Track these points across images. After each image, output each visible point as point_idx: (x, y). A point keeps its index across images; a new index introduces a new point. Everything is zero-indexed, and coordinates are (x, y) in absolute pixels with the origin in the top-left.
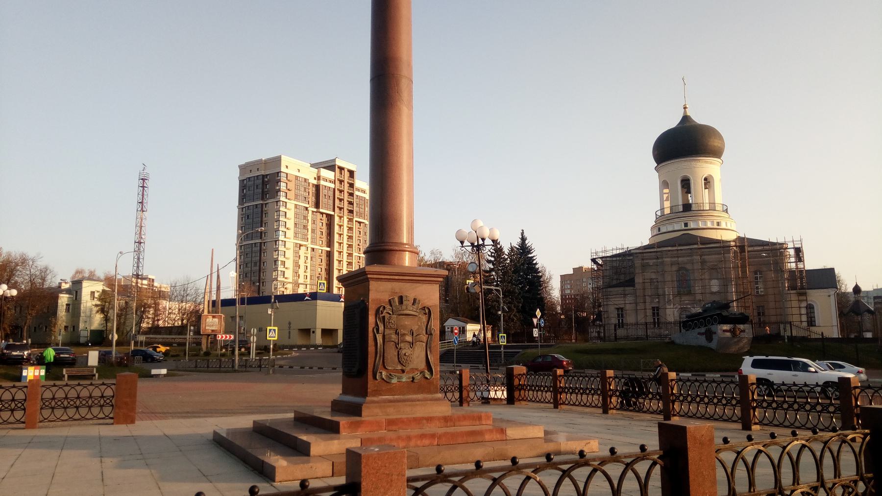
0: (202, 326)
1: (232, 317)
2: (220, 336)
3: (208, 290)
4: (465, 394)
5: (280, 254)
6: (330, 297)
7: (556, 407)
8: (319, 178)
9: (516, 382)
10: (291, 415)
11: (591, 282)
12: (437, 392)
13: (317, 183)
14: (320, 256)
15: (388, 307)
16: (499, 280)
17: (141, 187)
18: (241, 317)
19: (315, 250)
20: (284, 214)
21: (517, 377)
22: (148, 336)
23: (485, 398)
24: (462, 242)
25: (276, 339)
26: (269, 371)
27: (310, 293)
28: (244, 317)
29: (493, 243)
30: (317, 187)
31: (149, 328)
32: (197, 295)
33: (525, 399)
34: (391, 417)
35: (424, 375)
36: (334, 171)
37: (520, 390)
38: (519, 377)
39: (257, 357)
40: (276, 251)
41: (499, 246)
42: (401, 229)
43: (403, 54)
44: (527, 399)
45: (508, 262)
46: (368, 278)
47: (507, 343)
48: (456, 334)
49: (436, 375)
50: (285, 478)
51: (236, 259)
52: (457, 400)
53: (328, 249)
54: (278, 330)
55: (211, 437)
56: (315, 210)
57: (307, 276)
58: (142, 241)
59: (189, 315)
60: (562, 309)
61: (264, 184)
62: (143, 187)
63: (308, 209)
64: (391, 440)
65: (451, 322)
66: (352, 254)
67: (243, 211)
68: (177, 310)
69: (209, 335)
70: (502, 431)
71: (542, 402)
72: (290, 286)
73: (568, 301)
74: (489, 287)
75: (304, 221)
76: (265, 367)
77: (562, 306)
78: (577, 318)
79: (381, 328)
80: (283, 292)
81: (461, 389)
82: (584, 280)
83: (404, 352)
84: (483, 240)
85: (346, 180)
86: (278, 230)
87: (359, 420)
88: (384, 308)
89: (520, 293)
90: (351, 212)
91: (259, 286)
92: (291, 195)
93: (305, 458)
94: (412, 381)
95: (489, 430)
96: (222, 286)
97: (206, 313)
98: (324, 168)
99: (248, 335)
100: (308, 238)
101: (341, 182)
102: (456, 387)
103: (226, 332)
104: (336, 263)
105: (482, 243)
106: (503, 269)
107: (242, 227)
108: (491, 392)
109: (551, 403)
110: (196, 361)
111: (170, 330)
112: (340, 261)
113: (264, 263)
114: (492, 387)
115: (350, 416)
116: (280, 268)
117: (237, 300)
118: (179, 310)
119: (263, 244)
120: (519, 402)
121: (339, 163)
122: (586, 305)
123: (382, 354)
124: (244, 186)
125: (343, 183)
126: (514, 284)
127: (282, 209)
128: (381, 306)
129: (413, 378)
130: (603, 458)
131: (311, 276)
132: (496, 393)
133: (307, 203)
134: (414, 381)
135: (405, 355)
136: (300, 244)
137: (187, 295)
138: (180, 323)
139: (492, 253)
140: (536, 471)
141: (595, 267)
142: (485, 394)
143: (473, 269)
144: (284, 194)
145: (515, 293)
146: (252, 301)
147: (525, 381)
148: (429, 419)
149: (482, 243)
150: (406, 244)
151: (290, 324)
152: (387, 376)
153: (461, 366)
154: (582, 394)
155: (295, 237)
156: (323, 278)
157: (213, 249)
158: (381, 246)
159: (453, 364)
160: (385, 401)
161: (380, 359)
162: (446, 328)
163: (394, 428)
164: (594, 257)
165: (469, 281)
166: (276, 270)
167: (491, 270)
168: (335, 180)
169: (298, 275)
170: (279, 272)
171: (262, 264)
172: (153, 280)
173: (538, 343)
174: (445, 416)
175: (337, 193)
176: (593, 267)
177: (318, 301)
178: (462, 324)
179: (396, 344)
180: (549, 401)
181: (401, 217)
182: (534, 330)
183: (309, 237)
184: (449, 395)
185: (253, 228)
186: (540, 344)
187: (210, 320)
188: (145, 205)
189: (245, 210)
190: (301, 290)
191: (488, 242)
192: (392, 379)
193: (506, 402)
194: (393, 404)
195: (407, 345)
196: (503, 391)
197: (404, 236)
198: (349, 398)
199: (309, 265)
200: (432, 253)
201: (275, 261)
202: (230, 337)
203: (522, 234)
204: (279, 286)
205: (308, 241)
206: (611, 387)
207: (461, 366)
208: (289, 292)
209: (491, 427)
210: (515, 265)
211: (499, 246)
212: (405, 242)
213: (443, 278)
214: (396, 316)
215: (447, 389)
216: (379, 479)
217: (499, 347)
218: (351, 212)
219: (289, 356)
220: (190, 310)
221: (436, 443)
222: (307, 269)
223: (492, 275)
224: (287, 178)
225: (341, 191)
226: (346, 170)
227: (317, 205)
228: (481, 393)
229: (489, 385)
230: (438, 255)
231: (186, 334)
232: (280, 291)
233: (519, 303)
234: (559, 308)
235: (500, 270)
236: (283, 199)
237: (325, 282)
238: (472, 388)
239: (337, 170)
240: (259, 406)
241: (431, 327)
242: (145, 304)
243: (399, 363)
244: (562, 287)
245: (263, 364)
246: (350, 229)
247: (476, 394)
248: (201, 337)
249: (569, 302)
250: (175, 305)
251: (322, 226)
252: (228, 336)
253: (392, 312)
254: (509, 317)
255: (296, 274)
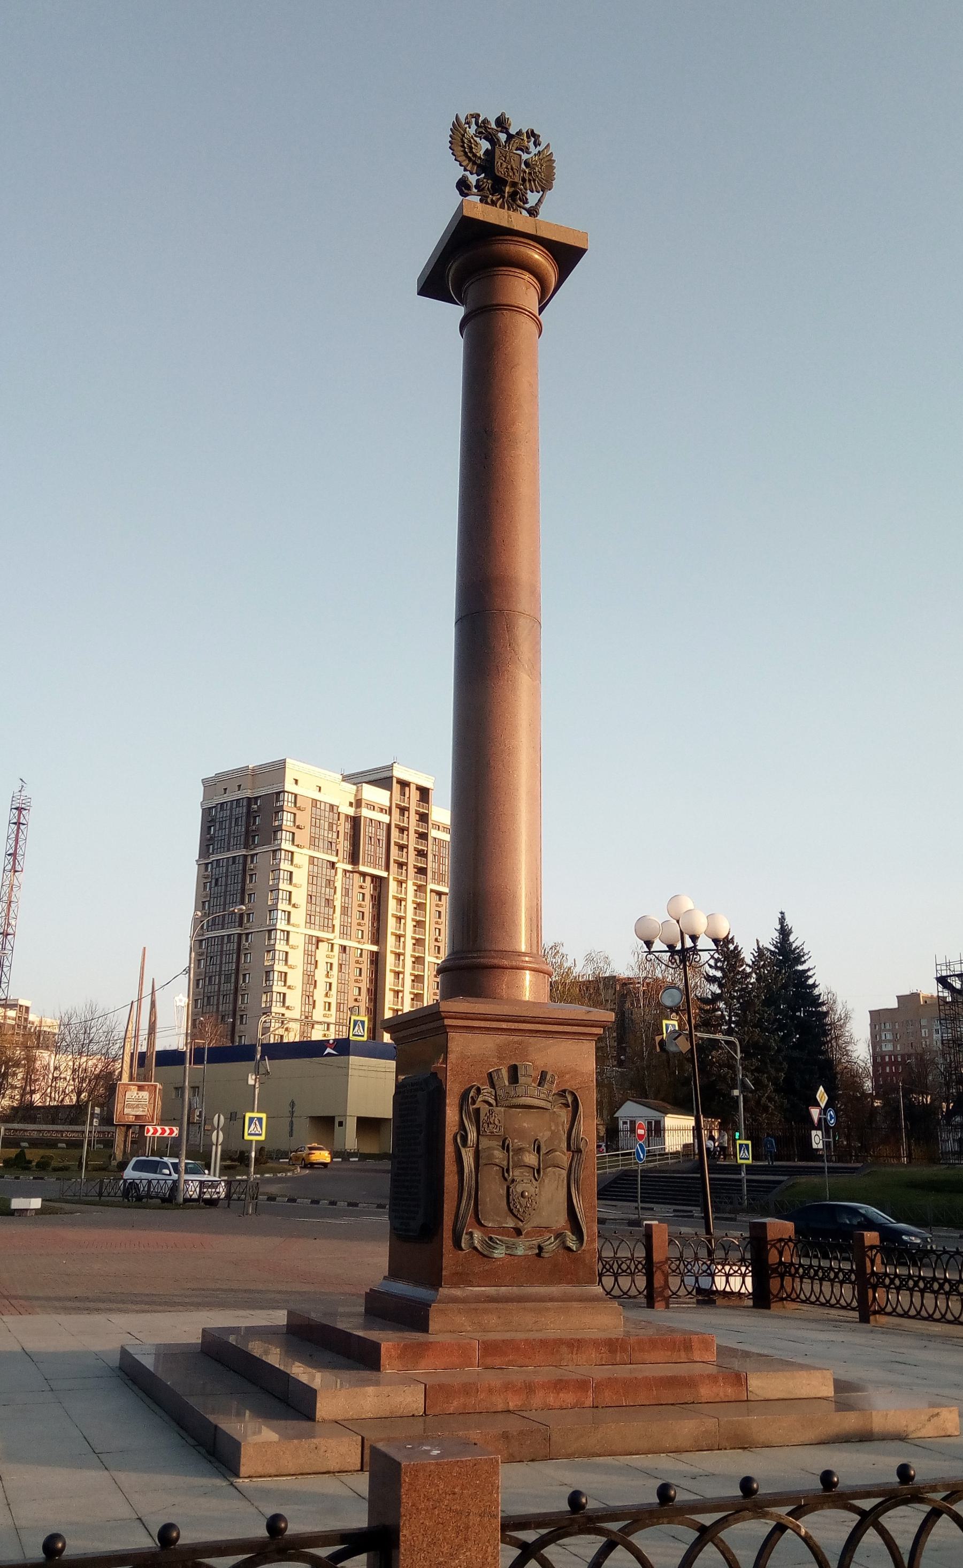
0: (118, 1107)
1: (176, 1088)
2: (150, 1128)
3: (131, 1033)
4: (658, 1280)
5: (277, 957)
6: (372, 1050)
7: (864, 1319)
8: (358, 803)
9: (773, 1257)
10: (280, 1318)
11: (939, 1027)
12: (592, 1282)
13: (356, 812)
14: (357, 962)
15: (486, 1089)
16: (733, 1019)
17: (15, 823)
18: (194, 1089)
19: (348, 949)
20: (287, 875)
21: (774, 1246)
22: (10, 1126)
23: (705, 1290)
24: (649, 944)
25: (262, 1138)
26: (245, 1207)
27: (335, 1040)
28: (201, 1089)
29: (716, 945)
30: (355, 821)
31: (13, 1108)
32: (110, 1042)
33: (794, 1296)
34: (492, 1336)
35: (564, 1242)
36: (389, 788)
37: (782, 1276)
38: (778, 1245)
39: (224, 1175)
40: (269, 951)
41: (731, 947)
42: (515, 923)
43: (522, 573)
44: (798, 1297)
45: (753, 980)
46: (445, 1026)
47: (753, 1159)
48: (641, 1137)
49: (591, 1243)
50: (260, 1470)
51: (189, 970)
52: (640, 1293)
53: (375, 948)
54: (267, 1118)
55: (115, 1361)
56: (349, 867)
57: (329, 1004)
58: (10, 931)
59: (93, 1083)
60: (876, 1087)
61: (250, 815)
62: (18, 824)
63: (337, 865)
64: (491, 1391)
65: (630, 1110)
66: (424, 958)
67: (206, 870)
68: (69, 1072)
69: (129, 1127)
70: (739, 1380)
71: (832, 1306)
72: (295, 1026)
73: (888, 1070)
74: (711, 1036)
75: (328, 890)
76: (239, 1199)
77: (876, 1077)
78: (910, 1106)
79: (472, 1136)
80: (282, 1036)
81: (649, 1268)
82: (924, 1023)
83: (519, 1189)
84: (694, 938)
85: (413, 807)
86: (273, 909)
87: (421, 1339)
88: (479, 1091)
89: (779, 1050)
90: (422, 871)
91: (234, 1024)
92: (303, 837)
93: (306, 1425)
94: (539, 1255)
95: (709, 1376)
96: (159, 1024)
97: (125, 1079)
98: (369, 783)
99: (207, 1127)
100: (334, 926)
101: (403, 810)
102: (640, 1262)
103: (163, 1121)
104: (389, 978)
105: (692, 945)
106: (740, 997)
107: (204, 902)
108: (717, 1279)
109: (853, 1309)
110: (102, 1182)
111: (54, 1114)
112: (397, 974)
113: (244, 975)
114: (720, 1267)
115: (401, 1330)
116: (278, 987)
117: (188, 1054)
118: (74, 1071)
119: (244, 937)
120: (779, 1304)
121: (399, 772)
122: (930, 1078)
123: (473, 1193)
124: (210, 819)
125: (406, 813)
126: (767, 1030)
127: (284, 865)
128: (472, 1087)
129: (540, 1248)
130: (955, 1485)
131: (339, 1004)
132: (727, 1281)
133: (335, 853)
134: (542, 1254)
135: (522, 1195)
136: (318, 937)
137: (90, 1042)
138: (75, 1099)
139: (717, 960)
140: (797, 1513)
141: (946, 994)
142: (704, 1282)
143: (672, 1001)
144: (289, 836)
145: (769, 1049)
146: (219, 1055)
147: (792, 1256)
148: (576, 1345)
149: (692, 945)
150: (525, 954)
151: (293, 1104)
152: (483, 1241)
153: (652, 1209)
154: (922, 1292)
155: (309, 923)
156: (363, 1010)
157: (145, 948)
158: (474, 958)
159: (635, 1204)
160: (478, 1299)
161: (468, 1204)
162: (621, 1123)
163: (497, 1361)
164: (944, 974)
165: (668, 1022)
166: (269, 990)
167: (716, 998)
168: (390, 808)
169: (311, 1002)
170: (275, 994)
171: (241, 977)
172: (27, 1008)
173: (823, 1161)
174: (610, 1339)
175: (395, 833)
176: (941, 994)
177: (351, 1058)
178: (653, 1114)
179: (505, 1171)
180: (849, 1305)
181: (515, 897)
182: (814, 1133)
183: (337, 923)
184: (625, 1282)
185: (225, 904)
186: (826, 1164)
187: (133, 1094)
188: (19, 858)
189: (212, 869)
190: (317, 1035)
191: (705, 943)
192: (495, 1248)
193: (750, 1303)
194: (495, 1305)
195: (528, 1175)
196: (744, 1276)
197: (520, 937)
198: (402, 1288)
199: (334, 981)
200: (589, 959)
201: (266, 972)
202: (172, 1132)
203: (782, 920)
204: (273, 1025)
205: (333, 931)
206: (875, 1269)
207: (652, 1209)
208: (292, 1036)
209: (712, 1370)
210: (768, 987)
211: (731, 947)
212: (523, 950)
213: (604, 1027)
214: (503, 1109)
215: (619, 1267)
216: (439, 1523)
217: (737, 1168)
218: (422, 871)
219: (289, 1174)
220: (96, 1073)
221: (589, 1402)
222: (330, 989)
223: (719, 1009)
224: (295, 803)
225: (402, 830)
226: (413, 787)
227: (354, 858)
228: (693, 1278)
229: (712, 1261)
230: (601, 965)
231: (84, 1123)
232: (275, 1035)
233: (778, 1070)
234: (868, 1085)
235: (734, 997)
236: (286, 845)
237: (366, 1019)
238: (673, 1266)
239: (396, 787)
240: (222, 1290)
241: (578, 1134)
242: (10, 1059)
243: (509, 1213)
244: (874, 1036)
245: (234, 1193)
246: (420, 906)
247: (682, 1281)
248: (112, 1129)
249: (891, 1069)
250: (65, 1061)
251: (363, 900)
252: (167, 1128)
253: (496, 1100)
254: (758, 1102)
255: (309, 1001)
